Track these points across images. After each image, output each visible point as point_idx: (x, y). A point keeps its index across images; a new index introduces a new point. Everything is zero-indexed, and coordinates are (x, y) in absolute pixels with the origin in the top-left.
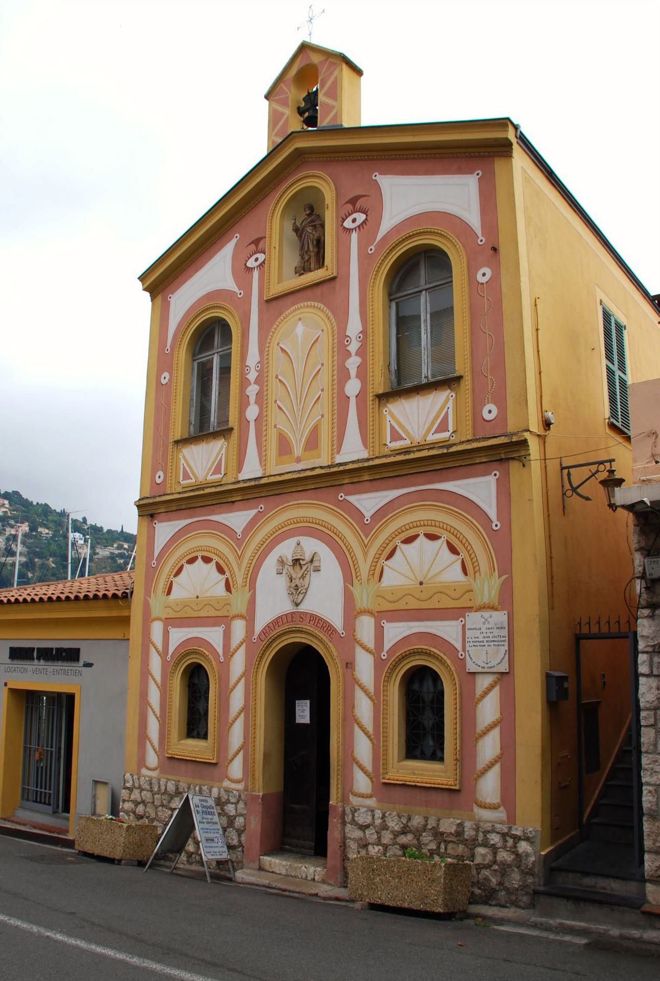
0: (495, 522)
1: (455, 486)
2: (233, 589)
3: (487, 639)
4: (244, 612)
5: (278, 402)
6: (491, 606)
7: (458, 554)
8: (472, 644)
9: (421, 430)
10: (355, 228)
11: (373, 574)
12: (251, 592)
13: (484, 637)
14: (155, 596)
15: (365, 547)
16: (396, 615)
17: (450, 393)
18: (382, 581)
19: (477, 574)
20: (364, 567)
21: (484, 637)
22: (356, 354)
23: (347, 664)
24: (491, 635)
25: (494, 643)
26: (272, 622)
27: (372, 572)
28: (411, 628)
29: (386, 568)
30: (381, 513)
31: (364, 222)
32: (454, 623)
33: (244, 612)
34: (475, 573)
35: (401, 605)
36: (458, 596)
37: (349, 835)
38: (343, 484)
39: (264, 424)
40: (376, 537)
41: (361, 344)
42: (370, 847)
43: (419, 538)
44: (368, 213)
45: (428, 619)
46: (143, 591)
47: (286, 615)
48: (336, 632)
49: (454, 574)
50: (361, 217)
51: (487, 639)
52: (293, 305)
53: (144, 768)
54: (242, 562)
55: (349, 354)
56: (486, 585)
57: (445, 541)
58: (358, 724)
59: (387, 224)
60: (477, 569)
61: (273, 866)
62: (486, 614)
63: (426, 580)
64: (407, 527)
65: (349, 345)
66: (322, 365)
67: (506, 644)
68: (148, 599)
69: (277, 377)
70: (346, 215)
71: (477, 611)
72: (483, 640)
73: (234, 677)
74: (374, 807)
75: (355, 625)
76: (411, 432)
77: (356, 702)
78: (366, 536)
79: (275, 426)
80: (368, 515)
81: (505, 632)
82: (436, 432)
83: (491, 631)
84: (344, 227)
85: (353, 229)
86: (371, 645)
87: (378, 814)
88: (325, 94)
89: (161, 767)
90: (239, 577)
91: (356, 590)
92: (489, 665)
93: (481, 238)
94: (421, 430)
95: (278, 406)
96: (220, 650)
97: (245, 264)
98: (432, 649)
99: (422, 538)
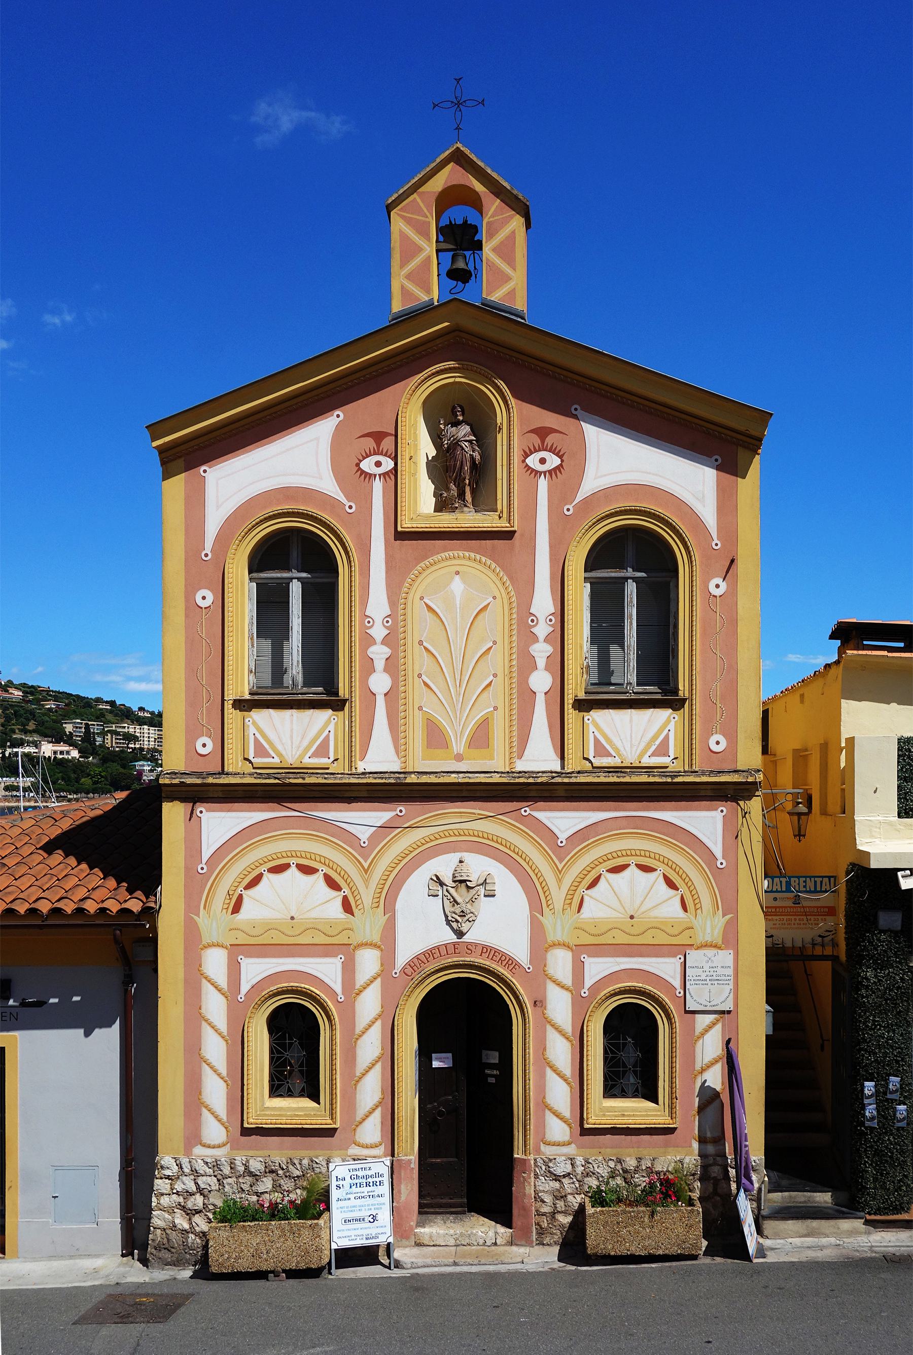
0: (720, 860)
1: (675, 817)
2: (355, 911)
3: (710, 978)
4: (376, 938)
5: (424, 677)
6: (713, 945)
7: (677, 889)
8: (693, 982)
9: (634, 749)
10: (545, 473)
11: (570, 904)
12: (387, 916)
13: (707, 976)
14: (208, 913)
15: (559, 873)
16: (600, 950)
17: (672, 714)
18: (582, 911)
19: (699, 911)
20: (558, 895)
21: (707, 976)
22: (546, 640)
23: (535, 1002)
24: (715, 974)
25: (718, 982)
26: (424, 953)
27: (568, 902)
28: (618, 964)
29: (586, 899)
30: (581, 836)
31: (558, 468)
32: (672, 960)
33: (376, 938)
34: (696, 910)
35: (607, 939)
36: (676, 933)
37: (541, 1188)
38: (528, 797)
39: (401, 702)
40: (574, 862)
41: (552, 629)
42: (570, 1198)
43: (629, 869)
44: (564, 458)
45: (641, 955)
46: (182, 906)
47: (446, 945)
48: (520, 966)
49: (673, 909)
50: (553, 461)
51: (710, 978)
52: (445, 550)
53: (199, 1146)
54: (370, 877)
55: (535, 639)
56: (709, 923)
57: (662, 875)
58: (551, 1067)
59: (590, 485)
60: (698, 906)
61: (434, 1239)
62: (710, 952)
63: (637, 914)
64: (615, 855)
65: (534, 626)
66: (495, 643)
67: (731, 983)
68: (195, 917)
69: (421, 643)
70: (530, 449)
71: (698, 948)
72: (706, 978)
73: (362, 1021)
74: (574, 1155)
75: (546, 959)
76: (621, 749)
77: (547, 1042)
78: (561, 861)
79: (420, 708)
80: (563, 837)
81: (730, 972)
82: (653, 755)
83: (715, 969)
84: (527, 465)
85: (541, 473)
86: (568, 981)
87: (580, 1161)
88: (494, 250)
89: (230, 1141)
90: (367, 895)
91: (547, 920)
92: (712, 1003)
93: (716, 541)
94: (634, 749)
95: (424, 682)
96: (338, 988)
97: (358, 465)
98: (647, 987)
99: (633, 869)
